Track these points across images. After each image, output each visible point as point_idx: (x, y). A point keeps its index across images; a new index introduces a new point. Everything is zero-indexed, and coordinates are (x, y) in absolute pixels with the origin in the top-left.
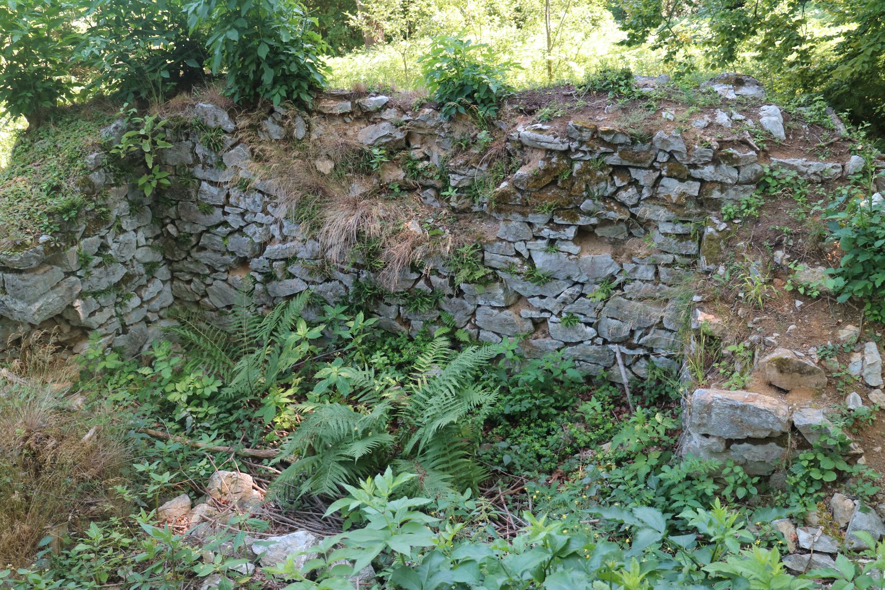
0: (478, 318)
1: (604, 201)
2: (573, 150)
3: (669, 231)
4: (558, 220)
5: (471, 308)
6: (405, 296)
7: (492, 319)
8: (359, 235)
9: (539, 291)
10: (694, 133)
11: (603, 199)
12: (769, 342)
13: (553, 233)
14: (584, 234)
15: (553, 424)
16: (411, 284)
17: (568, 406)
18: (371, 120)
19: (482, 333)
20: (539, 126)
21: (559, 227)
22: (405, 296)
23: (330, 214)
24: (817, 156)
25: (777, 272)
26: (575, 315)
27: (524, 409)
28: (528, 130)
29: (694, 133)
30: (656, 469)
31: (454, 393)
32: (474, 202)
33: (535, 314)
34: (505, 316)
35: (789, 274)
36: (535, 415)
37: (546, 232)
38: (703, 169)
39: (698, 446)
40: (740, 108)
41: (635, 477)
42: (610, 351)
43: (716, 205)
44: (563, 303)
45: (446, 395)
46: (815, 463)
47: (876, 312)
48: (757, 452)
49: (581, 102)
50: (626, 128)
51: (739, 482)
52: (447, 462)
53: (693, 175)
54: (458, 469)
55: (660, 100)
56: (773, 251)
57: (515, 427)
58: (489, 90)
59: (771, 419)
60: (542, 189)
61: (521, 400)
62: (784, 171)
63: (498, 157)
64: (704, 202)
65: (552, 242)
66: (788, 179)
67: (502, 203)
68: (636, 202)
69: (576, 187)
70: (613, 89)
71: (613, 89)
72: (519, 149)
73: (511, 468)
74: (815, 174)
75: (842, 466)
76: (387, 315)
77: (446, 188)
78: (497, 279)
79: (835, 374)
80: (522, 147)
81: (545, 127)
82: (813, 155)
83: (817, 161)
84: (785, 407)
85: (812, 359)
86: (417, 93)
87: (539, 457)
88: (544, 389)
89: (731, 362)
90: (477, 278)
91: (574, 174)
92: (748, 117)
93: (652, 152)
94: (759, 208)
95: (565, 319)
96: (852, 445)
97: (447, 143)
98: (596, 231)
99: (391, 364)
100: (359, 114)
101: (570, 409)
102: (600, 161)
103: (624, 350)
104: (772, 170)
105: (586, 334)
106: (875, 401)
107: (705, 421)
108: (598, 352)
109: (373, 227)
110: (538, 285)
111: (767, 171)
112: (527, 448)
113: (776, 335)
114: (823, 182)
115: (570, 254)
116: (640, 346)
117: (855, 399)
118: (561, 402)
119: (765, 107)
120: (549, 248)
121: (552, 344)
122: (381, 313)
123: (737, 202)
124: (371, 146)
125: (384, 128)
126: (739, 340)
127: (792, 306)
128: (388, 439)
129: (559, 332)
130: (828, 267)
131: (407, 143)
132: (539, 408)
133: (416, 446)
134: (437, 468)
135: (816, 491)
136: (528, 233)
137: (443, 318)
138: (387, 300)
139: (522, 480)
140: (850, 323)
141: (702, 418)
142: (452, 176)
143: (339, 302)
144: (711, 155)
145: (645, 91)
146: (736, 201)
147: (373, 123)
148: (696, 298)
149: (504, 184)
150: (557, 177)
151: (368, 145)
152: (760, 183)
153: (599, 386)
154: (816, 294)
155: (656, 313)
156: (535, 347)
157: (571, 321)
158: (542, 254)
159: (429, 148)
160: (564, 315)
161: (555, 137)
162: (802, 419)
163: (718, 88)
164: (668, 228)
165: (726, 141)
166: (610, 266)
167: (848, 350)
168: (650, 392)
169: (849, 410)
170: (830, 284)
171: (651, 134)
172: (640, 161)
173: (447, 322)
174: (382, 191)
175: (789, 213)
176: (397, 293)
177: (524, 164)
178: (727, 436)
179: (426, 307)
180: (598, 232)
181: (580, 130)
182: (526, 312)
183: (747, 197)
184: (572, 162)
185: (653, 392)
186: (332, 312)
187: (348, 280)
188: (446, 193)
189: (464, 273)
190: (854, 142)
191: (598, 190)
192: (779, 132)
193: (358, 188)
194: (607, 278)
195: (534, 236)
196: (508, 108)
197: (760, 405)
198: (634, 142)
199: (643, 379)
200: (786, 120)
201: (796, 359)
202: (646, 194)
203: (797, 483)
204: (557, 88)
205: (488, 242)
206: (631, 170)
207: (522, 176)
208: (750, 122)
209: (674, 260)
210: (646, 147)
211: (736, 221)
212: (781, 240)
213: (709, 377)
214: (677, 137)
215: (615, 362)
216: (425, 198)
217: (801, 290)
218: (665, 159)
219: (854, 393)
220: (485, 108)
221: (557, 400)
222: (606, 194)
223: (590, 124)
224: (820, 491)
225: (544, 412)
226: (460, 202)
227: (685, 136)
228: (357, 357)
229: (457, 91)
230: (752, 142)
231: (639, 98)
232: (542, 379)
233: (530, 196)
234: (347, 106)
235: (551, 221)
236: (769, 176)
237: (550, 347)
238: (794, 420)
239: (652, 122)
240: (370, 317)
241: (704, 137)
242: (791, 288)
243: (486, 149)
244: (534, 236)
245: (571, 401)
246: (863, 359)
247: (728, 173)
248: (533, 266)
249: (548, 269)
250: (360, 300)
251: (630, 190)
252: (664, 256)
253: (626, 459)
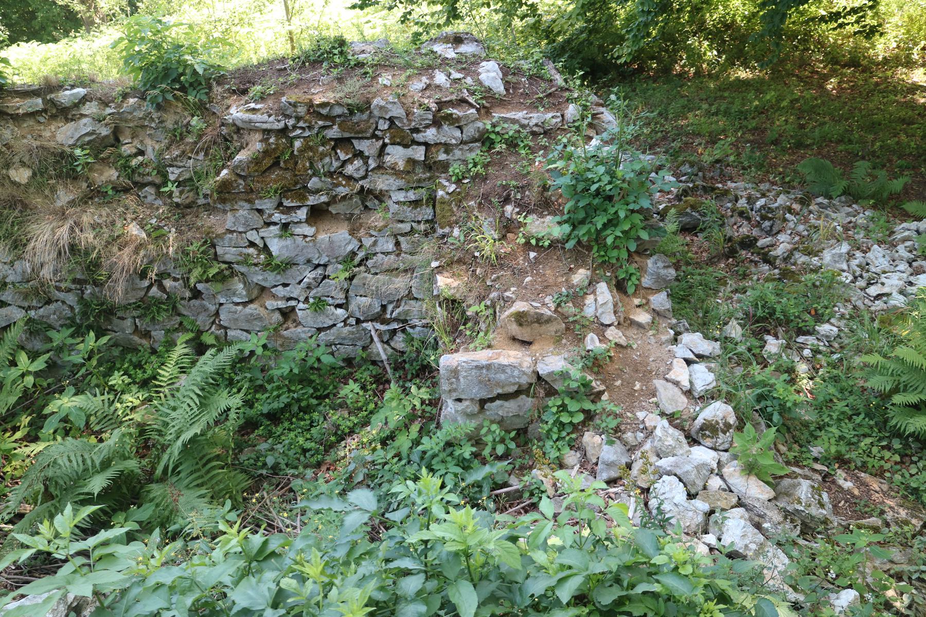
0: (222, 317)
1: (331, 177)
2: (291, 128)
3: (402, 200)
4: (287, 203)
5: (213, 308)
6: (139, 306)
7: (236, 316)
8: (73, 248)
9: (281, 279)
10: (412, 97)
11: (330, 174)
12: (508, 297)
13: (283, 217)
14: (317, 214)
15: (315, 415)
16: (143, 293)
17: (329, 394)
18: (70, 116)
19: (230, 333)
20: (252, 105)
21: (289, 210)
22: (139, 306)
23: (33, 228)
24: (537, 107)
25: (508, 228)
26: (323, 298)
27: (282, 405)
28: (241, 111)
29: (412, 97)
30: (417, 443)
31: (198, 403)
32: (198, 194)
33: (282, 304)
34: (251, 311)
35: (520, 228)
36: (295, 408)
37: (277, 217)
38: (425, 132)
39: (453, 412)
40: (459, 67)
41: (398, 455)
42: (365, 329)
43: (444, 166)
44: (308, 288)
45: (189, 405)
46: (563, 408)
47: (602, 253)
48: (508, 408)
49: (294, 76)
50: (341, 98)
51: (497, 439)
52: (199, 478)
53: (416, 140)
54: (214, 481)
55: (376, 65)
56: (503, 207)
57: (276, 426)
58: (195, 72)
59: (516, 373)
60: (265, 172)
61: (278, 396)
62: (506, 125)
63: (215, 143)
64: (433, 167)
65: (285, 226)
66: (511, 133)
67: (225, 192)
68: (364, 173)
69: (300, 166)
70: (327, 59)
71: (327, 59)
72: (235, 133)
73: (275, 469)
74: (536, 125)
75: (588, 406)
76: (123, 330)
77: (165, 184)
78: (233, 274)
79: (571, 319)
80: (238, 130)
81: (258, 106)
82: (533, 107)
83: (538, 112)
84: (529, 359)
85: (549, 308)
86: (120, 82)
87: (305, 451)
88: (303, 379)
89: (477, 323)
90: (210, 276)
91: (296, 153)
92: (467, 75)
93: (371, 121)
94: (486, 166)
95: (313, 304)
96: (593, 384)
97: (161, 135)
98: (330, 209)
99: (134, 383)
100: (54, 111)
101: (331, 396)
102: (320, 136)
103: (378, 326)
104: (494, 126)
105: (337, 317)
106: (611, 338)
107: (454, 386)
108: (353, 333)
109: (87, 237)
110: (279, 273)
111: (489, 127)
112: (291, 444)
113: (513, 289)
114: (546, 133)
115: (305, 236)
116: (396, 320)
117: (592, 339)
118: (322, 391)
119: (484, 63)
120: (283, 233)
121: (304, 332)
122: (115, 329)
123: (465, 162)
124: (73, 146)
125: (85, 125)
126: (481, 298)
127: (526, 258)
128: (133, 464)
129: (309, 319)
130: (556, 215)
131: (116, 138)
132: (298, 400)
133: (166, 468)
134: (191, 485)
135: (568, 434)
136: (258, 221)
137: (185, 323)
138: (119, 314)
139: (289, 479)
140: (581, 267)
141: (452, 384)
142: (170, 170)
143: (65, 325)
144: (431, 117)
145: (361, 57)
146: (464, 161)
147: (72, 120)
148: (434, 264)
149: (224, 172)
150: (279, 157)
151: (69, 146)
152: (485, 140)
153: (360, 366)
154: (547, 243)
155: (400, 283)
156: (287, 338)
157: (319, 305)
158: (276, 240)
159: (141, 141)
160: (311, 300)
161: (270, 116)
162: (545, 367)
163: (438, 48)
164: (400, 196)
165: (445, 102)
166: (350, 242)
167: (582, 294)
168: (412, 365)
169: (588, 351)
170: (558, 232)
171: (368, 102)
172: (361, 132)
173: (189, 327)
174: (95, 195)
175: (514, 166)
176: (130, 304)
177: (242, 148)
178: (479, 397)
179: (164, 314)
180: (333, 209)
181: (294, 105)
182: (271, 304)
183: (473, 155)
184: (291, 141)
185: (415, 364)
186: (58, 337)
187: (71, 299)
188: (166, 189)
189: (197, 272)
190: (571, 91)
191: (323, 166)
192: (499, 87)
193: (64, 196)
194: (348, 255)
195: (265, 223)
196: (217, 90)
197: (504, 361)
198: (351, 113)
199: (403, 353)
200: (505, 75)
201: (533, 311)
202: (372, 164)
203: (550, 430)
204: (270, 62)
205: (218, 236)
206: (354, 141)
207: (241, 161)
208: (469, 80)
209: (412, 227)
210: (365, 116)
211: (465, 181)
212: (509, 195)
213: (458, 341)
214: (395, 103)
215: (372, 340)
216: (145, 197)
217: (533, 242)
218: (386, 127)
219: (592, 334)
220: (195, 92)
221: (316, 390)
222: (332, 170)
223: (305, 98)
224: (572, 433)
225: (303, 404)
226: (183, 196)
227: (403, 100)
228: (94, 381)
229: (161, 75)
230: (471, 100)
231: (355, 65)
232: (296, 371)
233: (253, 181)
234: (38, 103)
235: (280, 204)
236: (493, 132)
237: (303, 336)
238: (538, 370)
239: (369, 89)
240: (104, 335)
241: (422, 100)
242: (523, 240)
243: (200, 137)
244: (265, 223)
245: (331, 387)
246: (596, 300)
247: (451, 134)
248: (270, 254)
249: (286, 255)
250: (88, 318)
251: (356, 162)
252: (400, 225)
253: (387, 438)
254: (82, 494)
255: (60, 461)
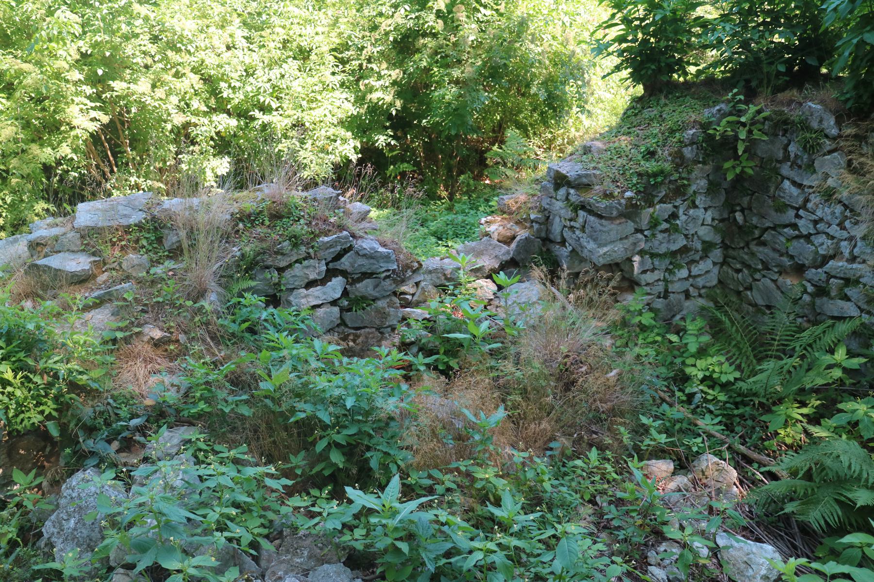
254: (845, 497)
255: (842, 458)
